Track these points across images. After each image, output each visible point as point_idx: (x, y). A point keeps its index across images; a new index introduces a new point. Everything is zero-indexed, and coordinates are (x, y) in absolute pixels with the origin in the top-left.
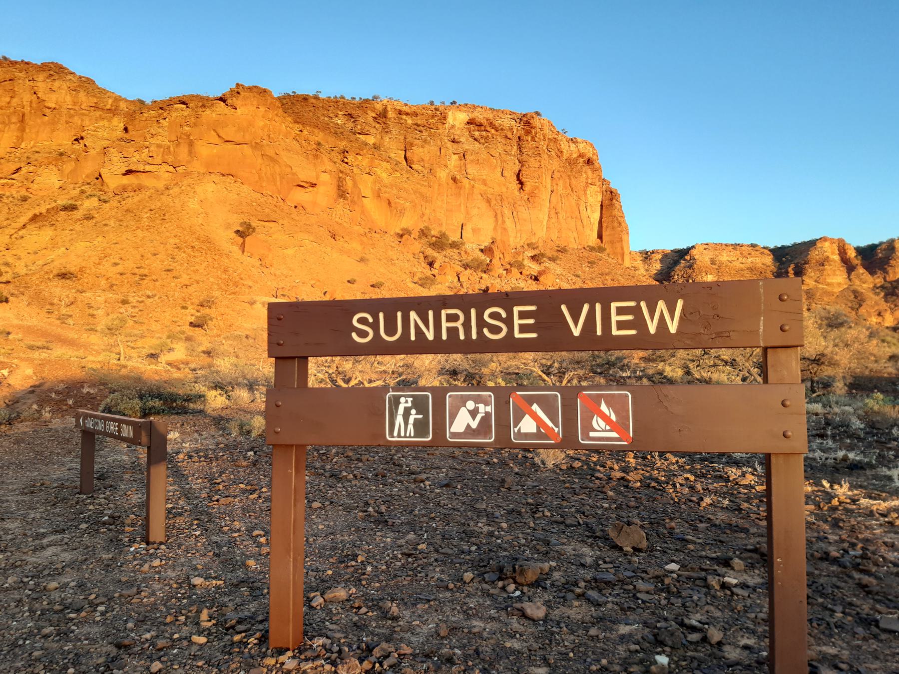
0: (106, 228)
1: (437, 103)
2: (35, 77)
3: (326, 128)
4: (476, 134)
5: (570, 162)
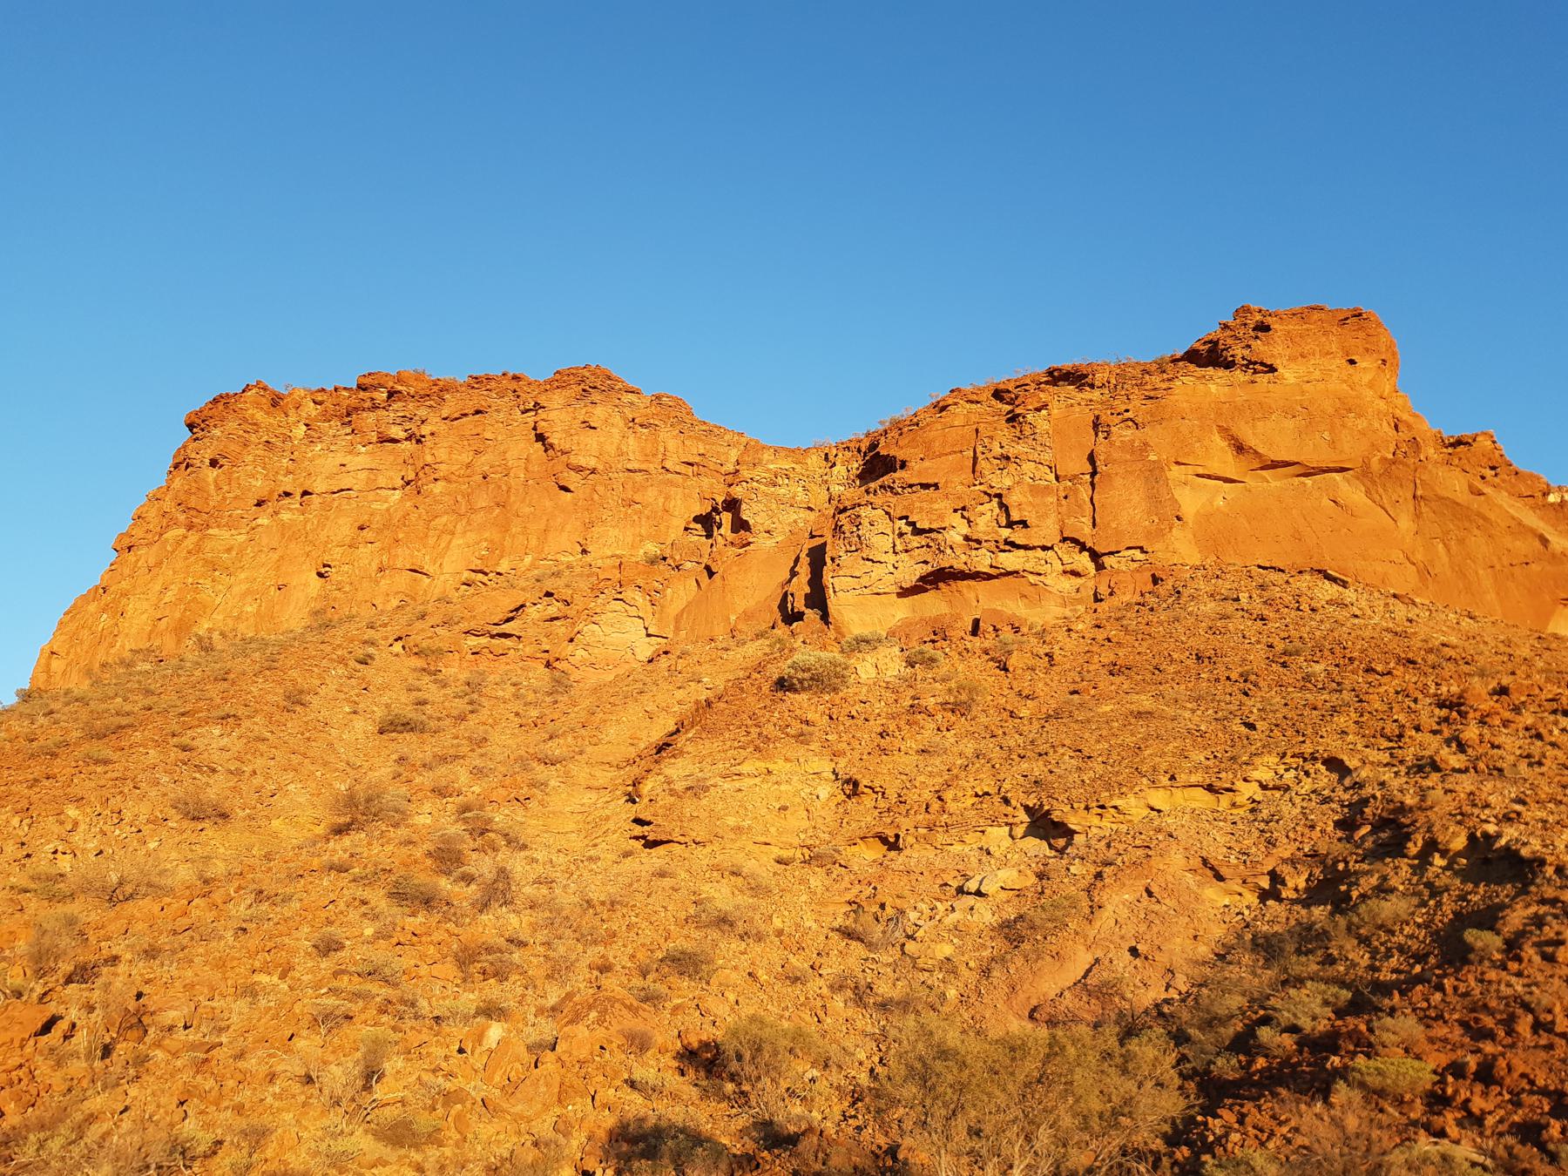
2: (542, 400)
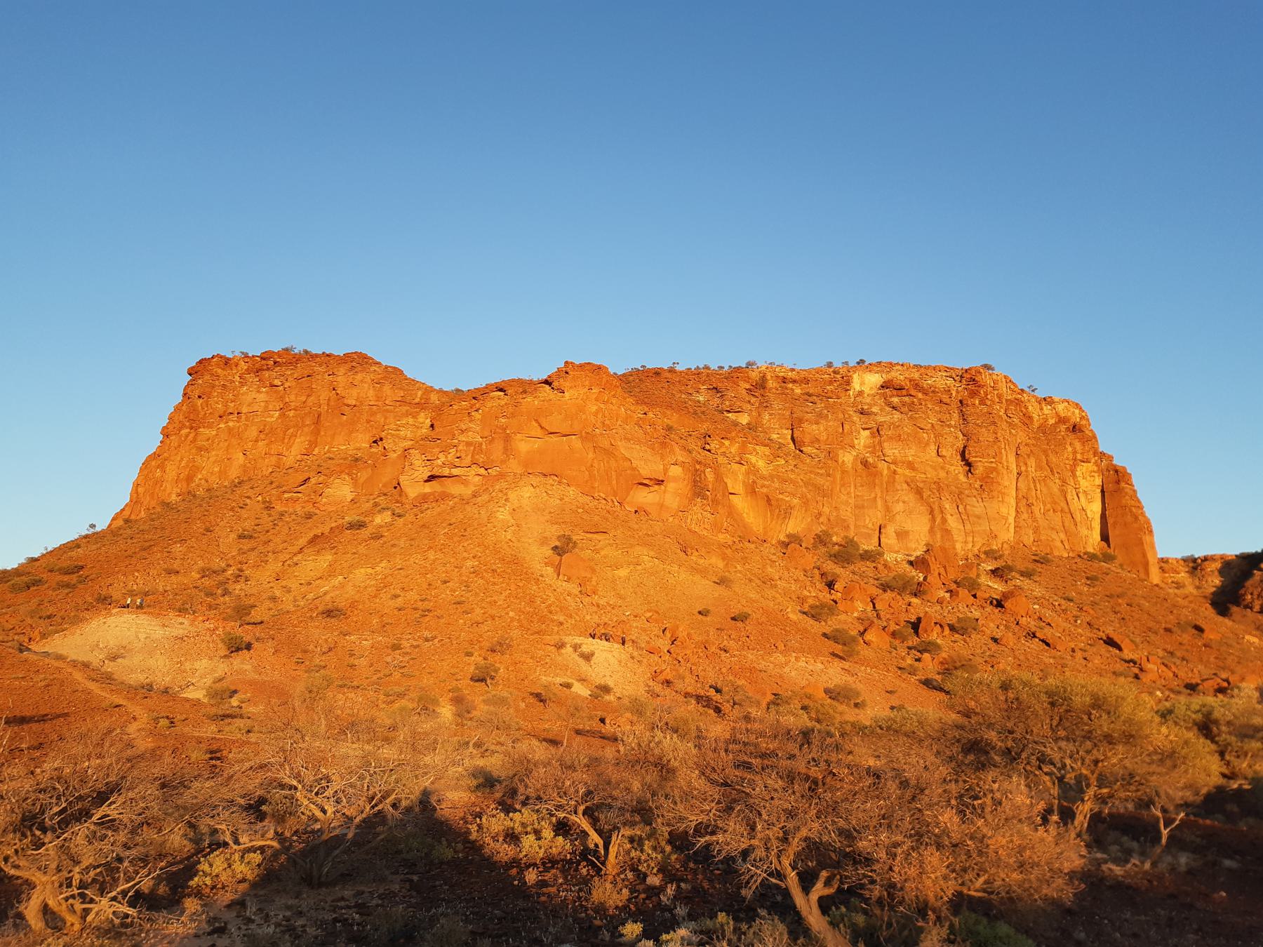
0: (394, 550)
1: (837, 364)
3: (682, 408)
4: (895, 400)
5: (1043, 429)
